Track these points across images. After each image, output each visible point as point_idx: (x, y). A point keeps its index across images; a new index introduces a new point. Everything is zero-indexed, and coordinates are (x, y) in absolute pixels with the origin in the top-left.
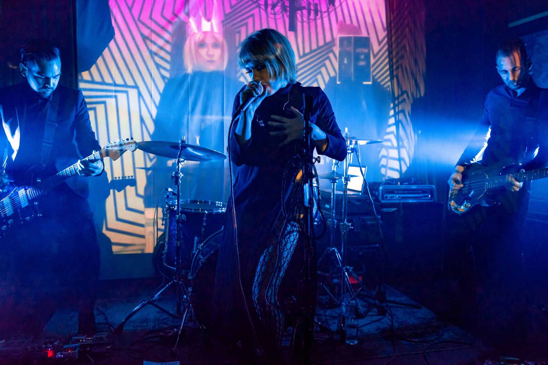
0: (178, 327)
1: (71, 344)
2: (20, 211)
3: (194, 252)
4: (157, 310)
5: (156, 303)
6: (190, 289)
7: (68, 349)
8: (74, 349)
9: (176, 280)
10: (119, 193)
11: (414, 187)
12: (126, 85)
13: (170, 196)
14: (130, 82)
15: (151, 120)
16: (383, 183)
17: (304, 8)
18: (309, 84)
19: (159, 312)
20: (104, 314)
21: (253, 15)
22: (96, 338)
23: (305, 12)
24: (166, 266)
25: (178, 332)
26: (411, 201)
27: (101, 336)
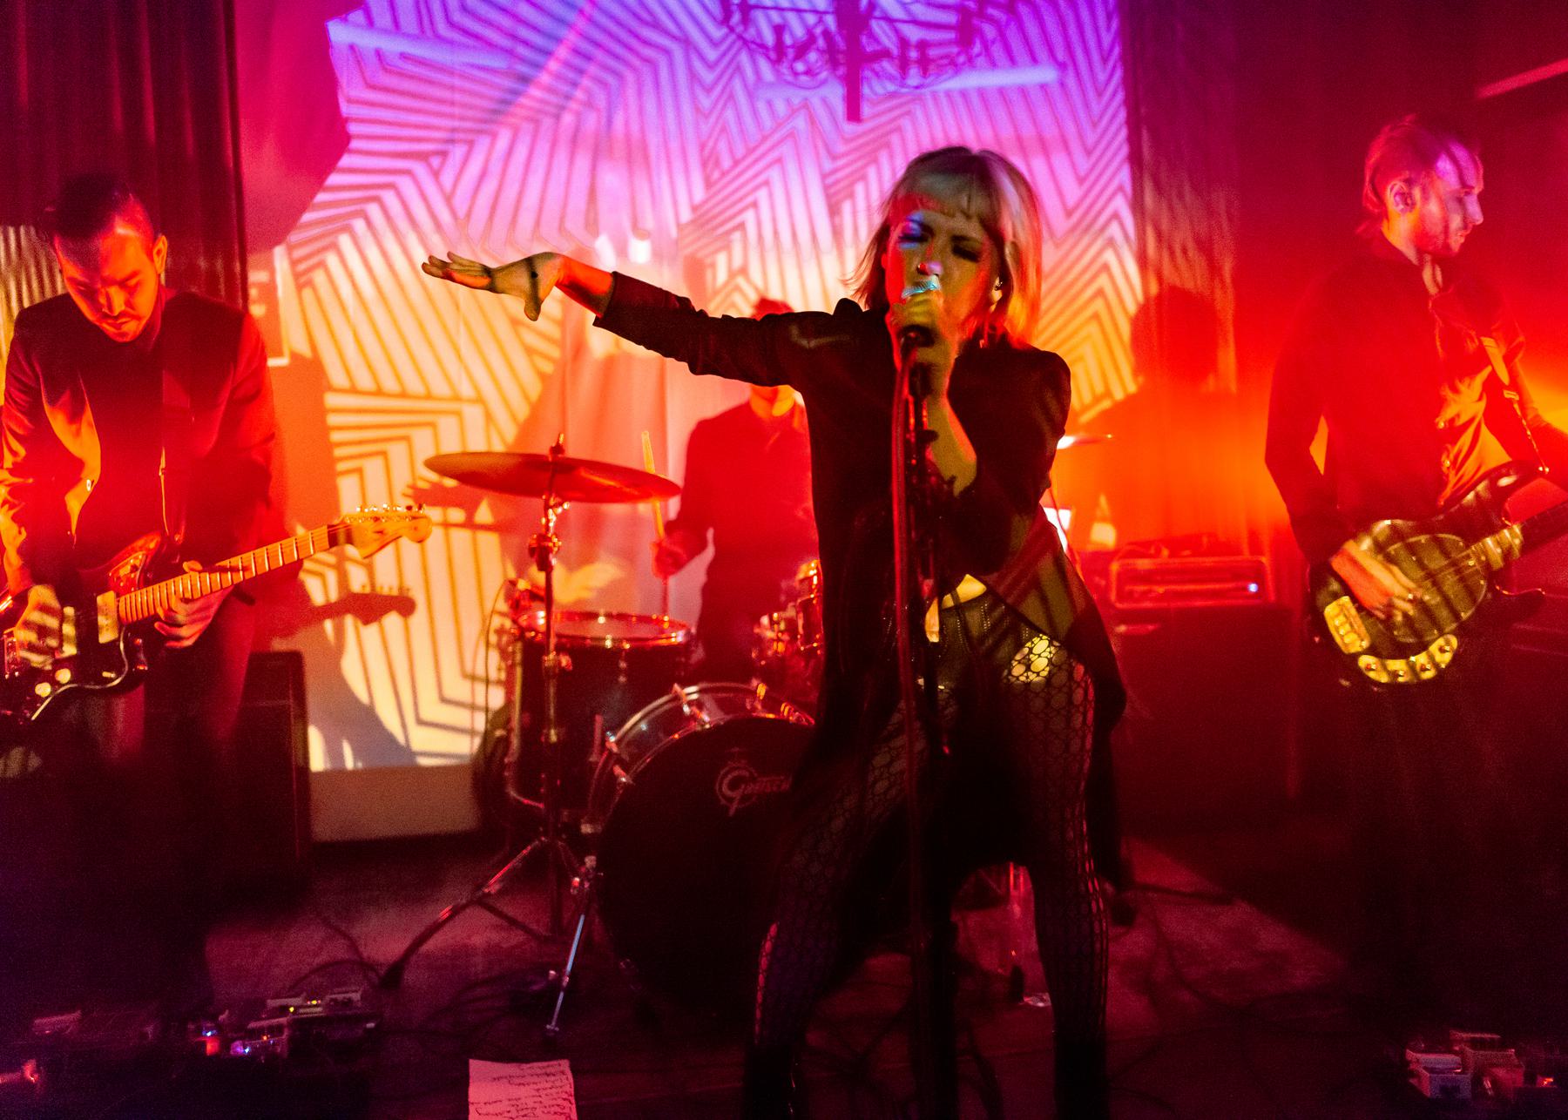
0: (560, 967)
1: (265, 1019)
3: (593, 759)
4: (495, 920)
5: (491, 901)
6: (590, 861)
7: (258, 1033)
8: (275, 1031)
9: (546, 836)
11: (1208, 561)
12: (457, 398)
13: (523, 603)
14: (466, 390)
16: (1120, 554)
19: (496, 927)
20: (345, 936)
21: (767, 183)
22: (332, 1000)
24: (518, 801)
25: (559, 978)
26: (1199, 603)
27: (347, 995)
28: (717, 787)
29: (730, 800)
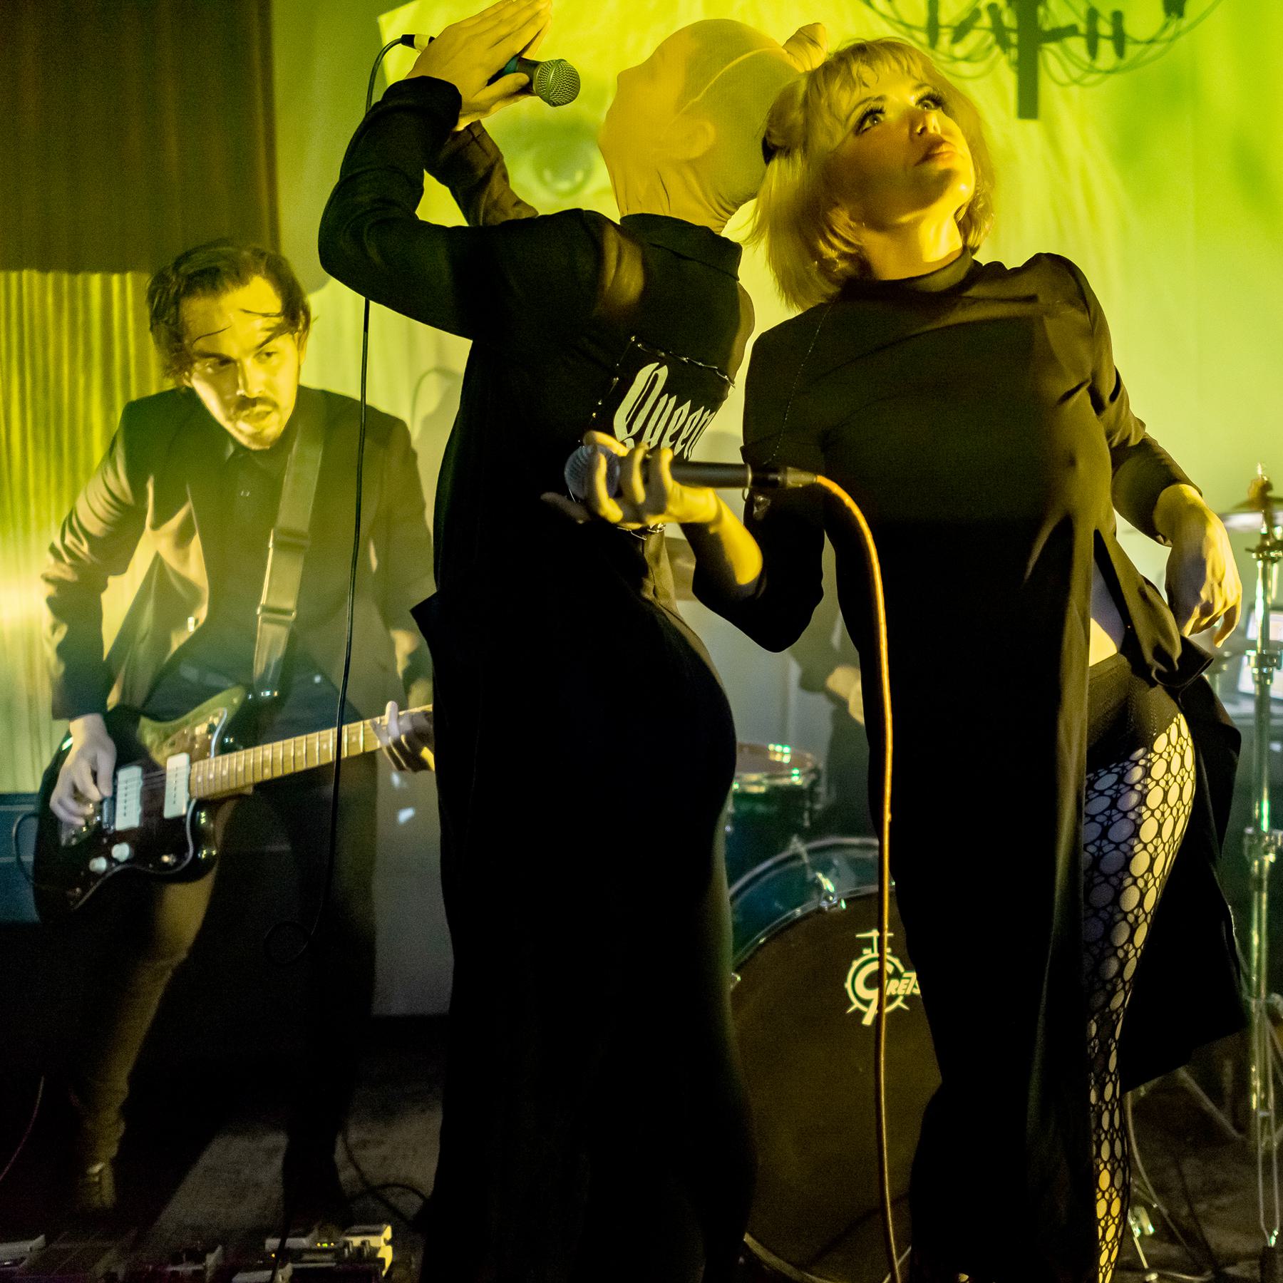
2: (108, 1183)
10: (384, 1257)
15: (248, 376)
17: (1072, 30)
18: (1121, 437)
23: (1077, 45)
28: (848, 985)
29: (867, 1003)
